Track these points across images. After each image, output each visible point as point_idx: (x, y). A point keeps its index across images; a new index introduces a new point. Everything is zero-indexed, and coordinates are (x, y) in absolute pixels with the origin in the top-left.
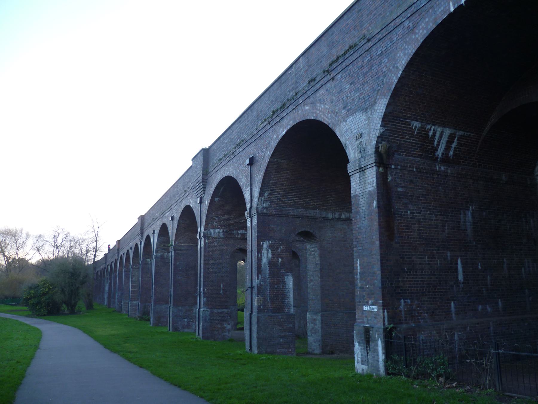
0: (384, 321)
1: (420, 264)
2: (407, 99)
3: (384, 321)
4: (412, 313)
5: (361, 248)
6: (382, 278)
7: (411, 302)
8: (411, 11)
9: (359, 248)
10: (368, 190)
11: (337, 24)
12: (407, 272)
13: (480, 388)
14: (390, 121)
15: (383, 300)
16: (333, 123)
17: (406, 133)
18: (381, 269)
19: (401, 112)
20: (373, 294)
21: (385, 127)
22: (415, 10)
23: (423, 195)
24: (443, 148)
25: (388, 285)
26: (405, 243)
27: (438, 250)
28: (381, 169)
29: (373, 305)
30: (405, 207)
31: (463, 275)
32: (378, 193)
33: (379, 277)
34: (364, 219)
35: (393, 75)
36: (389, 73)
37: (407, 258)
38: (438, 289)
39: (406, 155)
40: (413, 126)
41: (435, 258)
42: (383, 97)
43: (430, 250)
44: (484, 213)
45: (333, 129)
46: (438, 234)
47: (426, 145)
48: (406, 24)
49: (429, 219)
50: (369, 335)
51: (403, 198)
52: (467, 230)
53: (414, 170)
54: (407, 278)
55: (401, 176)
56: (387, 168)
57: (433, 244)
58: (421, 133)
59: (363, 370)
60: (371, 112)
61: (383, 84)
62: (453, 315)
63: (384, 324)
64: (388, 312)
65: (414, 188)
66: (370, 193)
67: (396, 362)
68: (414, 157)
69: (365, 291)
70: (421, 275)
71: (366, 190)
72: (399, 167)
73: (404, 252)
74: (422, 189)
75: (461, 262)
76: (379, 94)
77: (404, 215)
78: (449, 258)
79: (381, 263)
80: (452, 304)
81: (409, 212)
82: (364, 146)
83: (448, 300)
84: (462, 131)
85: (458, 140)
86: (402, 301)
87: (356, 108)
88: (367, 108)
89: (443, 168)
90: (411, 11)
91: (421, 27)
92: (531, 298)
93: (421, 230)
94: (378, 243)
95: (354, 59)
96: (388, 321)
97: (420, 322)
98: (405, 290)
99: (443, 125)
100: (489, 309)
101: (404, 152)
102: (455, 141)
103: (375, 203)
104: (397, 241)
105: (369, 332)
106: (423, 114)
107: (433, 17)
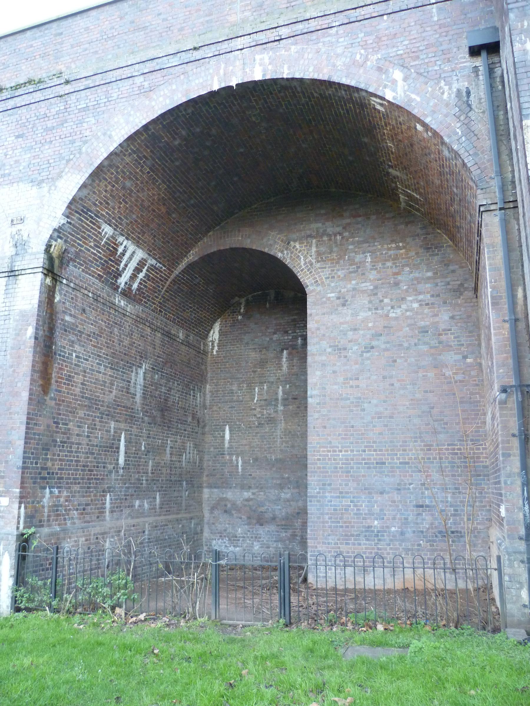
0: (18, 523)
1: (78, 435)
3: (18, 523)
7: (59, 492)
8: (150, 66)
11: (9, 39)
12: (59, 446)
13: (185, 617)
15: (21, 488)
17: (92, 238)
18: (26, 438)
19: (95, 205)
21: (68, 217)
22: (157, 68)
23: (94, 333)
25: (32, 463)
27: (102, 418)
28: (48, 280)
30: (70, 346)
31: (125, 457)
33: (20, 451)
35: (101, 145)
36: (93, 140)
37: (63, 424)
38: (94, 475)
39: (83, 270)
41: (96, 429)
42: (77, 172)
43: (92, 416)
44: (157, 376)
46: (104, 394)
47: (110, 264)
48: (139, 80)
49: (97, 372)
51: (69, 332)
52: (136, 395)
54: (59, 455)
55: (72, 298)
56: (56, 280)
57: (96, 409)
58: (109, 245)
61: (80, 153)
63: (18, 528)
64: (26, 508)
66: (23, 315)
67: (34, 589)
68: (93, 276)
70: (76, 452)
71: (15, 308)
72: (72, 285)
73: (60, 414)
74: (95, 326)
75: (125, 438)
76: (70, 165)
77: (68, 358)
78: (112, 431)
79: (27, 428)
81: (74, 355)
82: (25, 238)
83: (103, 492)
84: (156, 259)
85: (147, 270)
86: (48, 490)
87: (21, 175)
89: (122, 303)
90: (150, 66)
91: (162, 93)
92: (187, 493)
93: (85, 385)
94: (25, 395)
95: (33, 101)
96: (25, 522)
97: (66, 524)
98: (53, 473)
99: (138, 243)
100: (146, 506)
101: (82, 265)
102: (144, 270)
103: (30, 331)
106: (120, 218)
107: (185, 86)
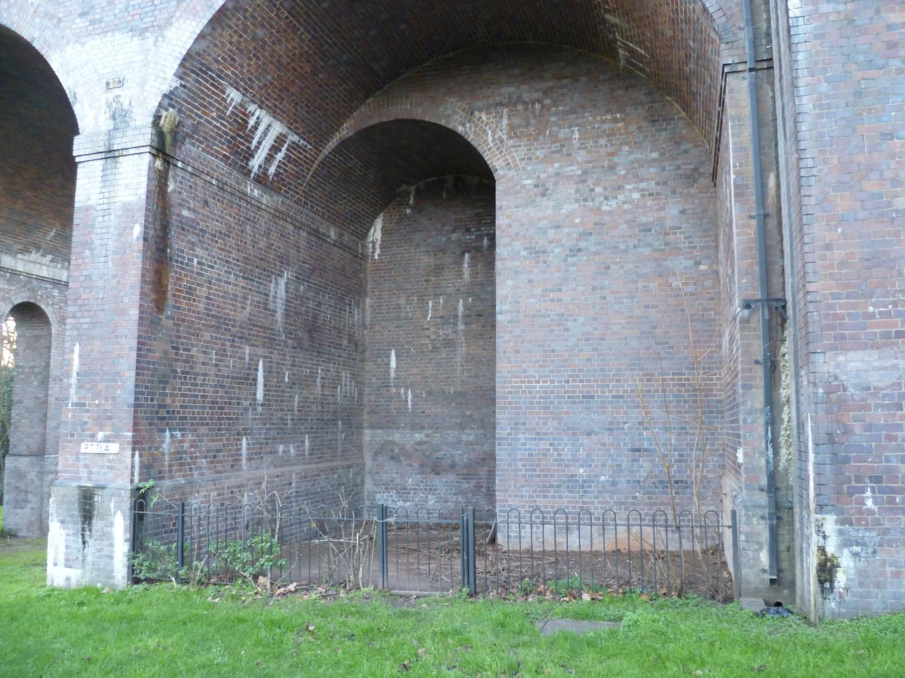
1: (203, 364)
2: (236, 38)
3: (133, 475)
4: (181, 458)
5: (88, 320)
6: (137, 386)
7: (183, 435)
9: (82, 320)
10: (123, 199)
12: (180, 378)
13: (345, 587)
14: (193, 71)
16: (45, 41)
17: (214, 106)
18: (137, 368)
19: (217, 61)
20: (110, 418)
21: (181, 78)
24: (264, 155)
25: (146, 400)
26: (183, 320)
27: (233, 341)
28: (158, 163)
29: (107, 440)
30: (189, 249)
31: (264, 391)
32: (147, 209)
34: (103, 259)
37: (184, 350)
39: (204, 150)
40: (229, 95)
42: (191, 17)
43: (220, 339)
45: (43, 52)
46: (235, 311)
50: (92, 505)
52: (276, 312)
53: (214, 182)
54: (180, 389)
55: (191, 187)
57: (226, 330)
58: (237, 116)
59: (68, 579)
60: (156, 42)
62: (244, 462)
63: (132, 481)
64: (141, 456)
65: (208, 217)
66: (127, 208)
67: (155, 556)
68: (217, 157)
69: (88, 411)
70: (202, 385)
71: (116, 200)
72: (190, 169)
73: (180, 337)
74: (221, 223)
75: (264, 366)
76: (182, 8)
77: (187, 265)
78: (247, 357)
79: (139, 355)
80: (244, 441)
81: (195, 260)
82: (126, 106)
83: (238, 434)
84: (298, 134)
85: (287, 150)
86: (168, 433)
87: (116, 21)
88: (146, 29)
89: (256, 193)
92: (343, 435)
94: (134, 313)
96: (141, 474)
97: (192, 475)
98: (173, 412)
99: (275, 113)
101: (202, 143)
102: (284, 149)
103: (137, 230)
104: (169, 313)
105: (91, 498)
106: (250, 79)
